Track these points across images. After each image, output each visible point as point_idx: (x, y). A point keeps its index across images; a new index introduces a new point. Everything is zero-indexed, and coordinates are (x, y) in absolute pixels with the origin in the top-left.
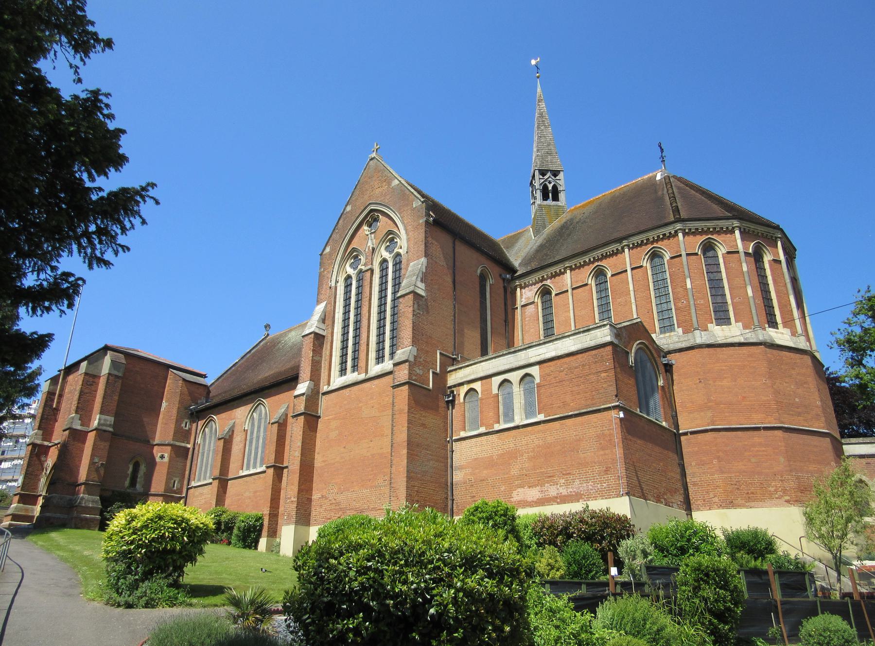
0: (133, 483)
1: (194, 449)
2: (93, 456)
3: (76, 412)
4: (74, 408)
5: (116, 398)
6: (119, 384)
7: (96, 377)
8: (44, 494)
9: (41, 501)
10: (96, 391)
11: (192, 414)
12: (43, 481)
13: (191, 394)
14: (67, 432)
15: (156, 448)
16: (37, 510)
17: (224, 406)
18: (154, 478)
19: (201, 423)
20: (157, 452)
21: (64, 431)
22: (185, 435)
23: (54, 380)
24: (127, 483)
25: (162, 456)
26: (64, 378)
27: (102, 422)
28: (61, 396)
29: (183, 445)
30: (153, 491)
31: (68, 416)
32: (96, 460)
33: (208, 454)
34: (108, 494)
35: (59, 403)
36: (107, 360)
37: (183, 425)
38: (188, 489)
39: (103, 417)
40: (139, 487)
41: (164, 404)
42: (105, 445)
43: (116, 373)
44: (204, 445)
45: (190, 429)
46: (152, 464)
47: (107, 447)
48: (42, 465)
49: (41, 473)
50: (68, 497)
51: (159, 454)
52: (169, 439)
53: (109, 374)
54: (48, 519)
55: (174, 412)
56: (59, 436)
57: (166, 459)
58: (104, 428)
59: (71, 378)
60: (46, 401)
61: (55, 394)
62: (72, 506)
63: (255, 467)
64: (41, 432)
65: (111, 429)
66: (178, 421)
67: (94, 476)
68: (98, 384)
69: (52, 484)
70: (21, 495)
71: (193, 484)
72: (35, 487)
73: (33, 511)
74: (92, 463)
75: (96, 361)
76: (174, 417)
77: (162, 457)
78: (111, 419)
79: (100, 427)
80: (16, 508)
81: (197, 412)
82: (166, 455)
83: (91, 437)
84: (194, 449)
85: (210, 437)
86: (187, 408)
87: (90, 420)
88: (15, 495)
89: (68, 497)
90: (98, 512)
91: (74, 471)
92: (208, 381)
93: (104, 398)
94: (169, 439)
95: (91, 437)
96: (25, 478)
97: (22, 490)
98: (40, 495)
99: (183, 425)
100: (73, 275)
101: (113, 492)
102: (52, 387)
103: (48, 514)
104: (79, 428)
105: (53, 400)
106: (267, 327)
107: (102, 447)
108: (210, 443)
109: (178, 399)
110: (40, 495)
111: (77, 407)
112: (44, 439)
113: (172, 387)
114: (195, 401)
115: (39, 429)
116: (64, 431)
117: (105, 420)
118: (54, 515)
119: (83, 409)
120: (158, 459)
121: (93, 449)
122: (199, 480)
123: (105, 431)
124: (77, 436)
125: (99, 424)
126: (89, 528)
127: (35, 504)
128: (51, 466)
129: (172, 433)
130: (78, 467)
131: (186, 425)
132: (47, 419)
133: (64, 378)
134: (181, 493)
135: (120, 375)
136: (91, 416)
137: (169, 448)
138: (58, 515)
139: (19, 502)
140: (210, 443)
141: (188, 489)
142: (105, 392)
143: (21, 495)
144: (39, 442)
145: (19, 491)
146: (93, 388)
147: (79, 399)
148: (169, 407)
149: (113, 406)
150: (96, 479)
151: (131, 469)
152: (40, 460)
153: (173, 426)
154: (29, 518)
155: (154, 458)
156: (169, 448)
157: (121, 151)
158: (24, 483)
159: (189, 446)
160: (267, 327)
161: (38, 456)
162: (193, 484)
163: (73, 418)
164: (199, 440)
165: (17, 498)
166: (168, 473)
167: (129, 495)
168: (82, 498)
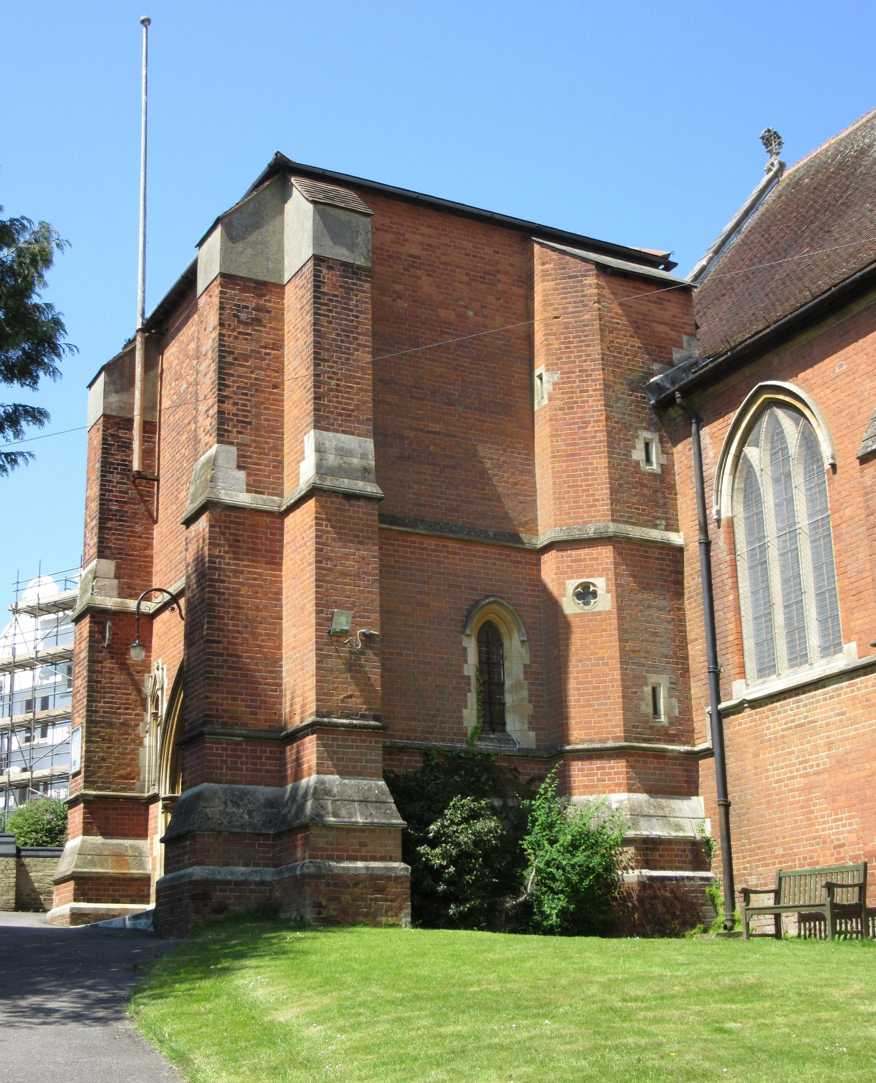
0: (493, 716)
1: (707, 545)
2: (324, 607)
3: (222, 437)
4: (207, 423)
5: (365, 357)
6: (363, 296)
7: (267, 289)
8: (164, 791)
9: (159, 820)
10: (278, 345)
11: (664, 405)
12: (152, 746)
13: (639, 325)
14: (203, 523)
15: (549, 561)
16: (151, 856)
17: (832, 323)
18: (572, 685)
19: (713, 435)
20: (558, 576)
21: (189, 522)
22: (652, 495)
23: (117, 372)
24: (470, 716)
25: (586, 590)
26: (150, 364)
27: (332, 459)
28: (150, 428)
29: (655, 534)
30: (579, 736)
31: (191, 464)
32: (342, 622)
33: (790, 556)
34: (412, 765)
35: (149, 453)
36: (298, 212)
37: (638, 455)
38: (721, 716)
39: (334, 439)
40: (518, 729)
41: (546, 383)
42: (362, 558)
43: (341, 254)
44: (756, 522)
45: (667, 470)
46: (551, 632)
47: (374, 566)
48: (138, 688)
49: (140, 717)
50: (264, 791)
51: (572, 585)
52: (598, 519)
53: (318, 260)
54: (202, 891)
55: (594, 403)
56: (173, 553)
57: (605, 601)
58: (346, 484)
59: (172, 354)
60: (106, 451)
61: (128, 423)
62: (287, 827)
63: (798, 657)
64: (109, 566)
65: (372, 489)
66: (617, 440)
67: (346, 691)
68: (279, 317)
69: (189, 742)
70: (90, 803)
71: (740, 690)
72: (132, 775)
73: (139, 857)
74: (328, 638)
75: (257, 226)
76: (597, 430)
77: (585, 593)
78: (361, 448)
79: (329, 483)
80: (82, 852)
81: (688, 391)
82: (600, 584)
83: (300, 532)
84: (707, 545)
85: (783, 479)
86: (638, 385)
87: (279, 465)
88: (72, 803)
89: (264, 791)
90: (395, 845)
91: (261, 686)
92: (683, 274)
93: (318, 359)
94: (598, 519)
95: (300, 532)
96: (89, 739)
97: (88, 783)
98: (154, 799)
99: (638, 455)
100: (132, 341)
101: (426, 754)
102: (114, 398)
103: (198, 872)
104: (244, 499)
105: (128, 446)
106: (771, 140)
107: (351, 565)
108: (786, 503)
109: (596, 350)
110: (154, 799)
111: (222, 417)
112: (125, 592)
113: (560, 301)
114: (658, 350)
115: (102, 553)
116: (189, 522)
117: (342, 452)
118: (223, 873)
119: (245, 417)
120: (570, 606)
121: (320, 580)
122: (767, 669)
123: (350, 496)
124: (242, 535)
125: (321, 469)
126: (372, 920)
127: (142, 832)
128: (168, 685)
129: (603, 492)
130: (275, 662)
131: (646, 451)
132: (121, 516)
133: (150, 364)
134: (686, 734)
135: (360, 262)
136: (278, 449)
137: (606, 554)
138: (240, 871)
139: (86, 832)
140: (786, 503)
141: (721, 716)
142: (318, 333)
143: (90, 803)
144: (110, 602)
145: (77, 787)
146: (267, 337)
147: (222, 384)
148: (566, 393)
149: (361, 391)
150: (358, 703)
151: (472, 657)
152: (124, 666)
153: (600, 463)
154: (135, 887)
155: (552, 605)
156: (606, 554)
157: (163, 845)
158: (89, 759)
159: (676, 539)
160: (771, 140)
161: (118, 652)
162: (740, 690)
163: (213, 463)
164: (725, 503)
165: (76, 817)
166: (626, 658)
167: (485, 762)
168: (320, 792)
